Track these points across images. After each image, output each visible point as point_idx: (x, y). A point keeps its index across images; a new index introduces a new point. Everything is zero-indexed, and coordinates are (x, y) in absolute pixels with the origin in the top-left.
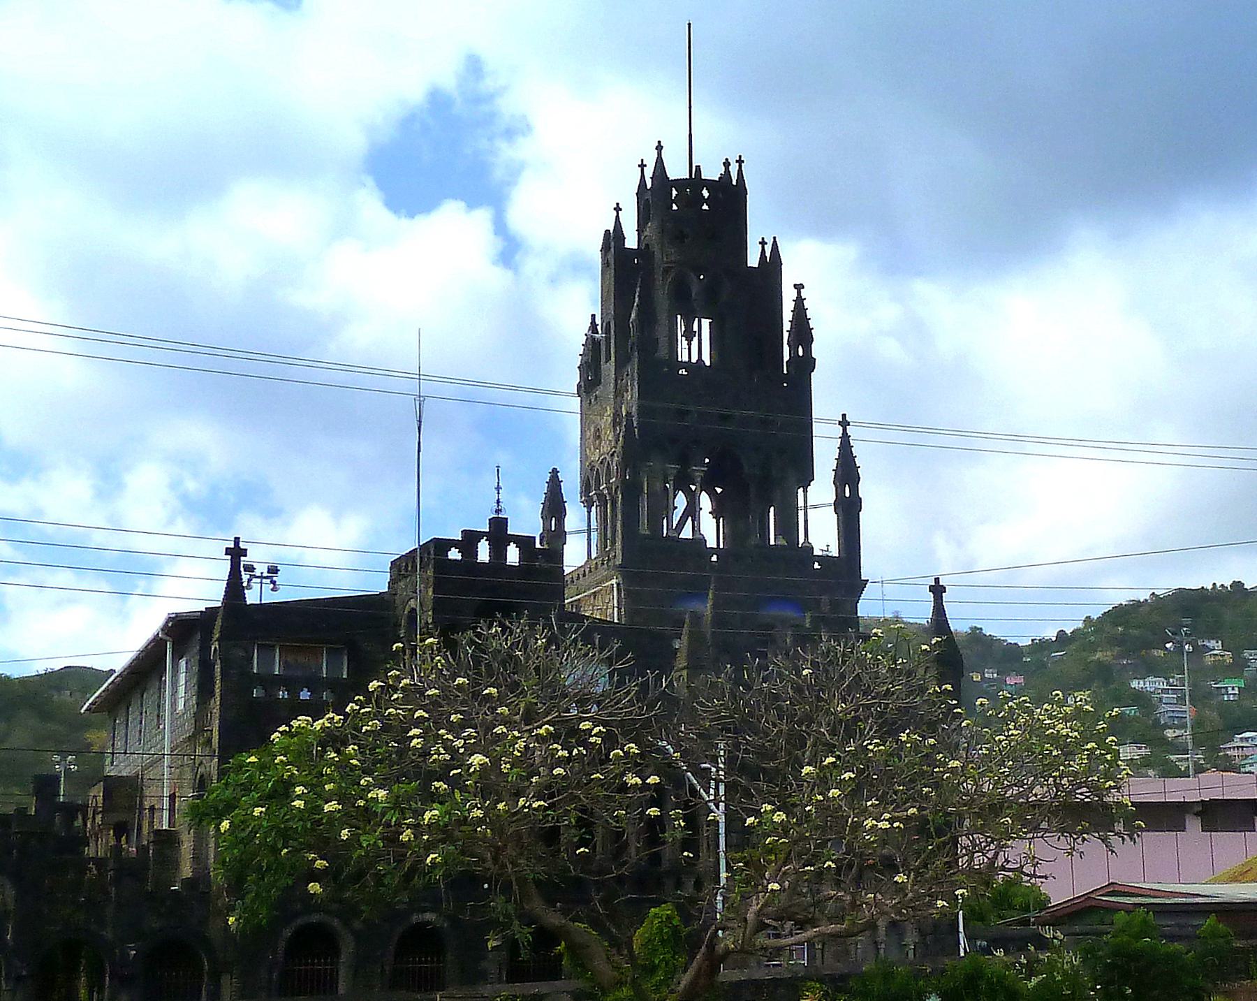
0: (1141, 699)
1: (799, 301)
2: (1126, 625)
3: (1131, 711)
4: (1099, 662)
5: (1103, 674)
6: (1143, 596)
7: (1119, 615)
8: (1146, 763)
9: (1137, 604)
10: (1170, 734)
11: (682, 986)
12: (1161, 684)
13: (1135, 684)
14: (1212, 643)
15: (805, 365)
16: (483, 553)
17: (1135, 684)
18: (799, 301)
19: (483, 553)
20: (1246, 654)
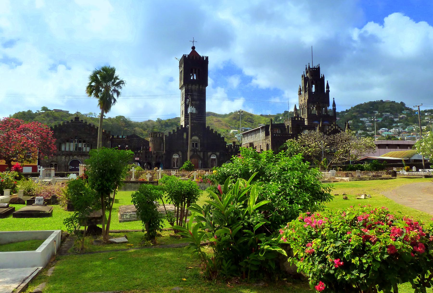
0: (362, 122)
1: (327, 83)
2: (359, 108)
3: (360, 124)
4: (354, 115)
5: (355, 117)
6: (363, 103)
7: (358, 106)
8: (363, 134)
9: (362, 104)
10: (368, 128)
11: (374, 174)
12: (366, 119)
13: (361, 119)
14: (376, 112)
15: (328, 91)
16: (296, 119)
17: (361, 119)
18: (327, 83)
19: (296, 119)
20: (383, 113)
